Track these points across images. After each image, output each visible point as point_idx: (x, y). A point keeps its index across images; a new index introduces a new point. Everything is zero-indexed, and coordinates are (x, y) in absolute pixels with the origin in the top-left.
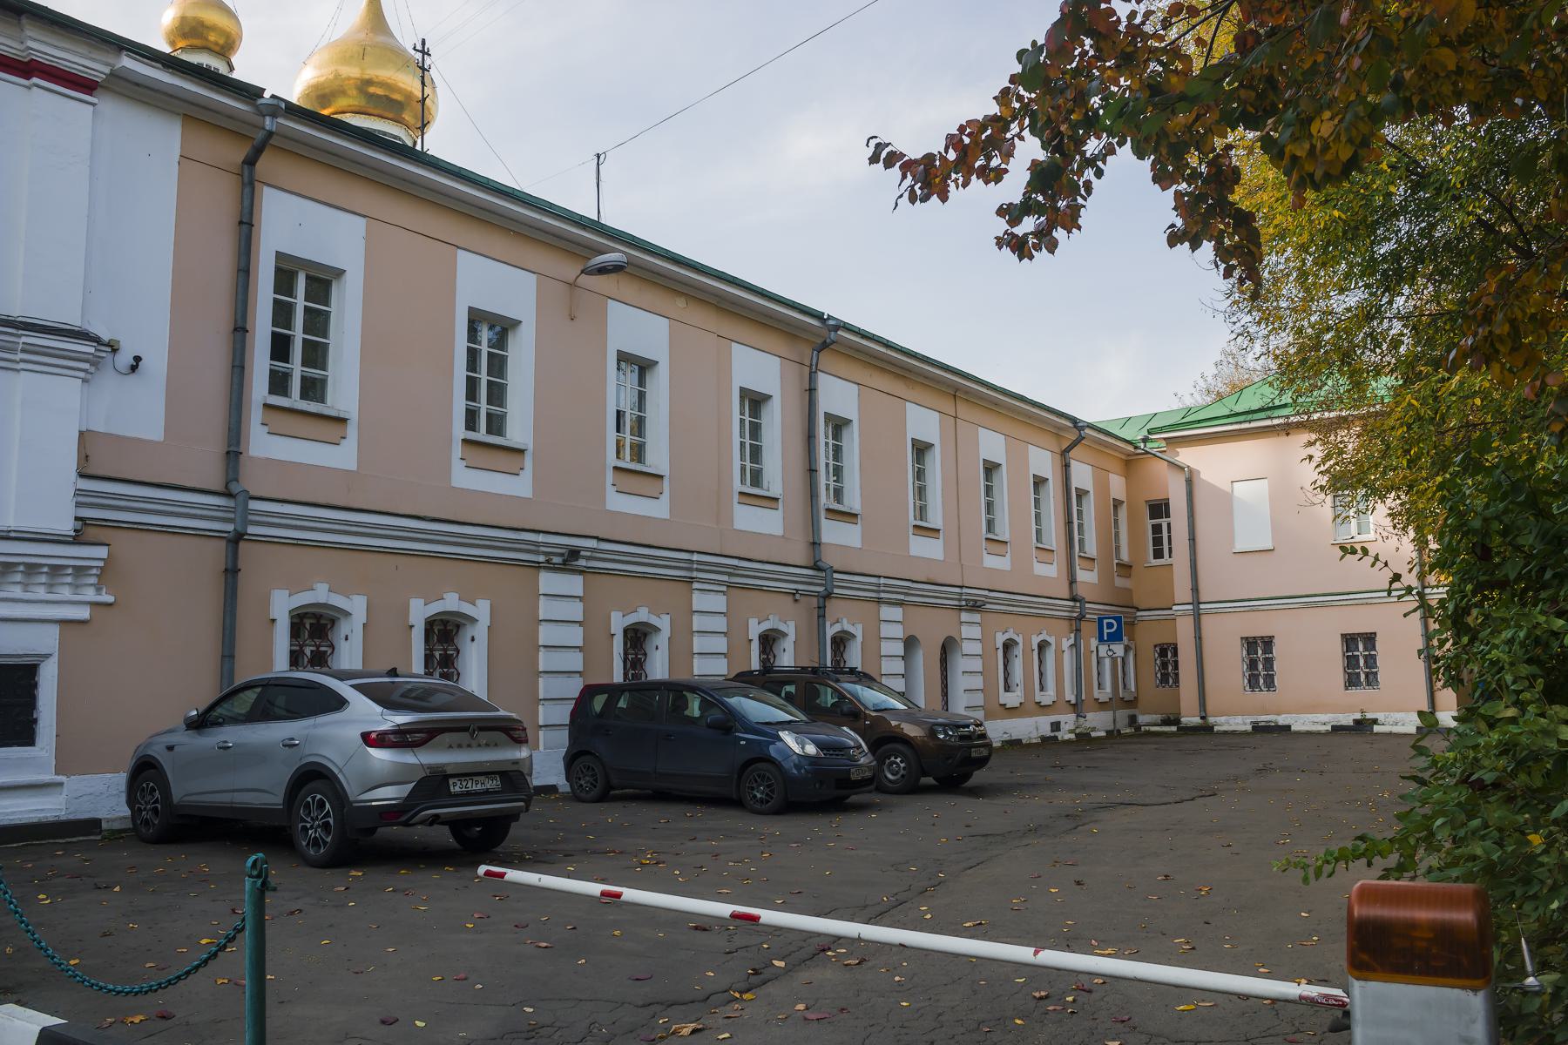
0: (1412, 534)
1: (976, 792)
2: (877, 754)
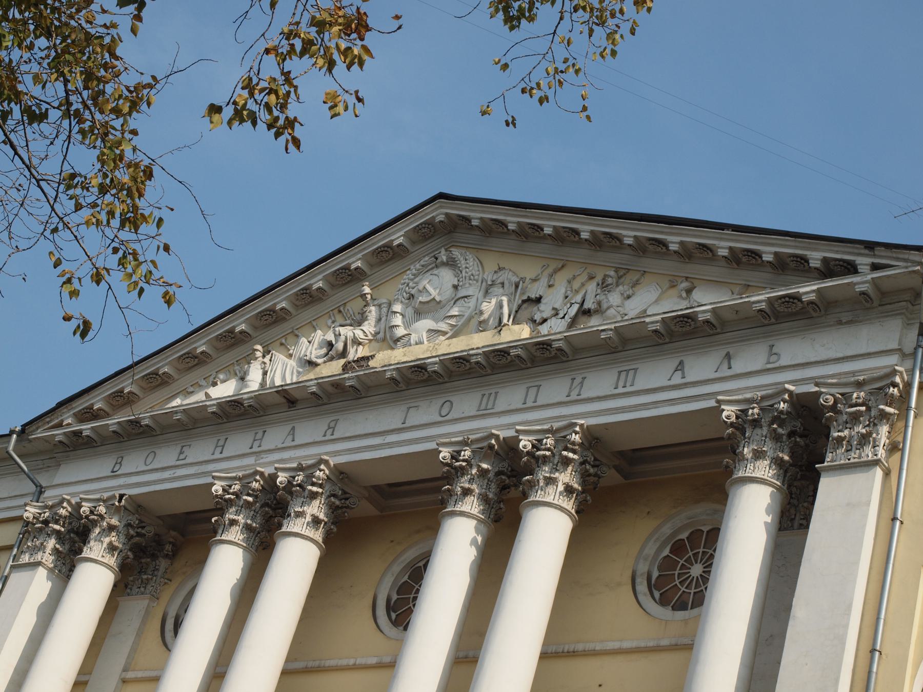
1: (724, 358)
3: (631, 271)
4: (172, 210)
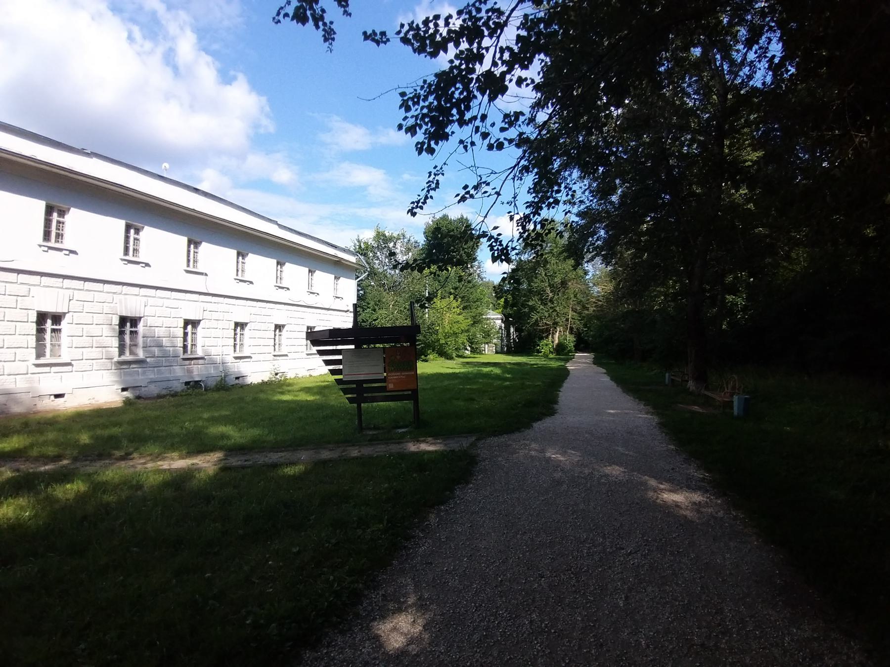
2: (142, 225)
3: (70, 313)
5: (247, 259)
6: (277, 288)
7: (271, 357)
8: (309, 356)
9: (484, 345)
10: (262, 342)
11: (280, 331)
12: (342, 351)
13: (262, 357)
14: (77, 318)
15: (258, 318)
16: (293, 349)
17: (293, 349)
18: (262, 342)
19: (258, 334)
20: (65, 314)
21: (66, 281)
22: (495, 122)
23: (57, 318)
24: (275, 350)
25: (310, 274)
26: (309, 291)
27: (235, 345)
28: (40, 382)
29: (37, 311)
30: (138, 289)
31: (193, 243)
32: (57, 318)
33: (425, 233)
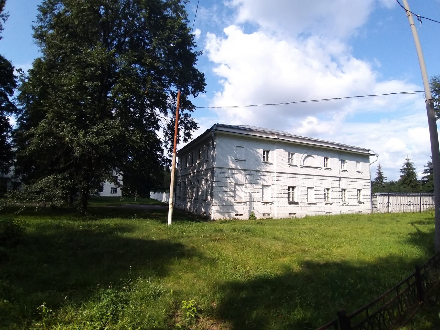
0: (61, 308)
4: (33, 22)
5: (328, 160)
6: (325, 169)
7: (324, 204)
8: (310, 205)
9: (422, 210)
10: (353, 197)
11: (344, 191)
12: (177, 206)
13: (353, 204)
14: (349, 190)
15: (350, 187)
16: (351, 200)
17: (351, 200)
18: (353, 197)
19: (351, 193)
20: (346, 189)
21: (283, 174)
22: (32, 21)
23: (293, 188)
24: (325, 201)
25: (326, 160)
26: (325, 167)
27: (325, 198)
28: (34, 21)
29: (288, 186)
30: (287, 174)
31: (291, 154)
32: (293, 188)
33: (243, 33)
